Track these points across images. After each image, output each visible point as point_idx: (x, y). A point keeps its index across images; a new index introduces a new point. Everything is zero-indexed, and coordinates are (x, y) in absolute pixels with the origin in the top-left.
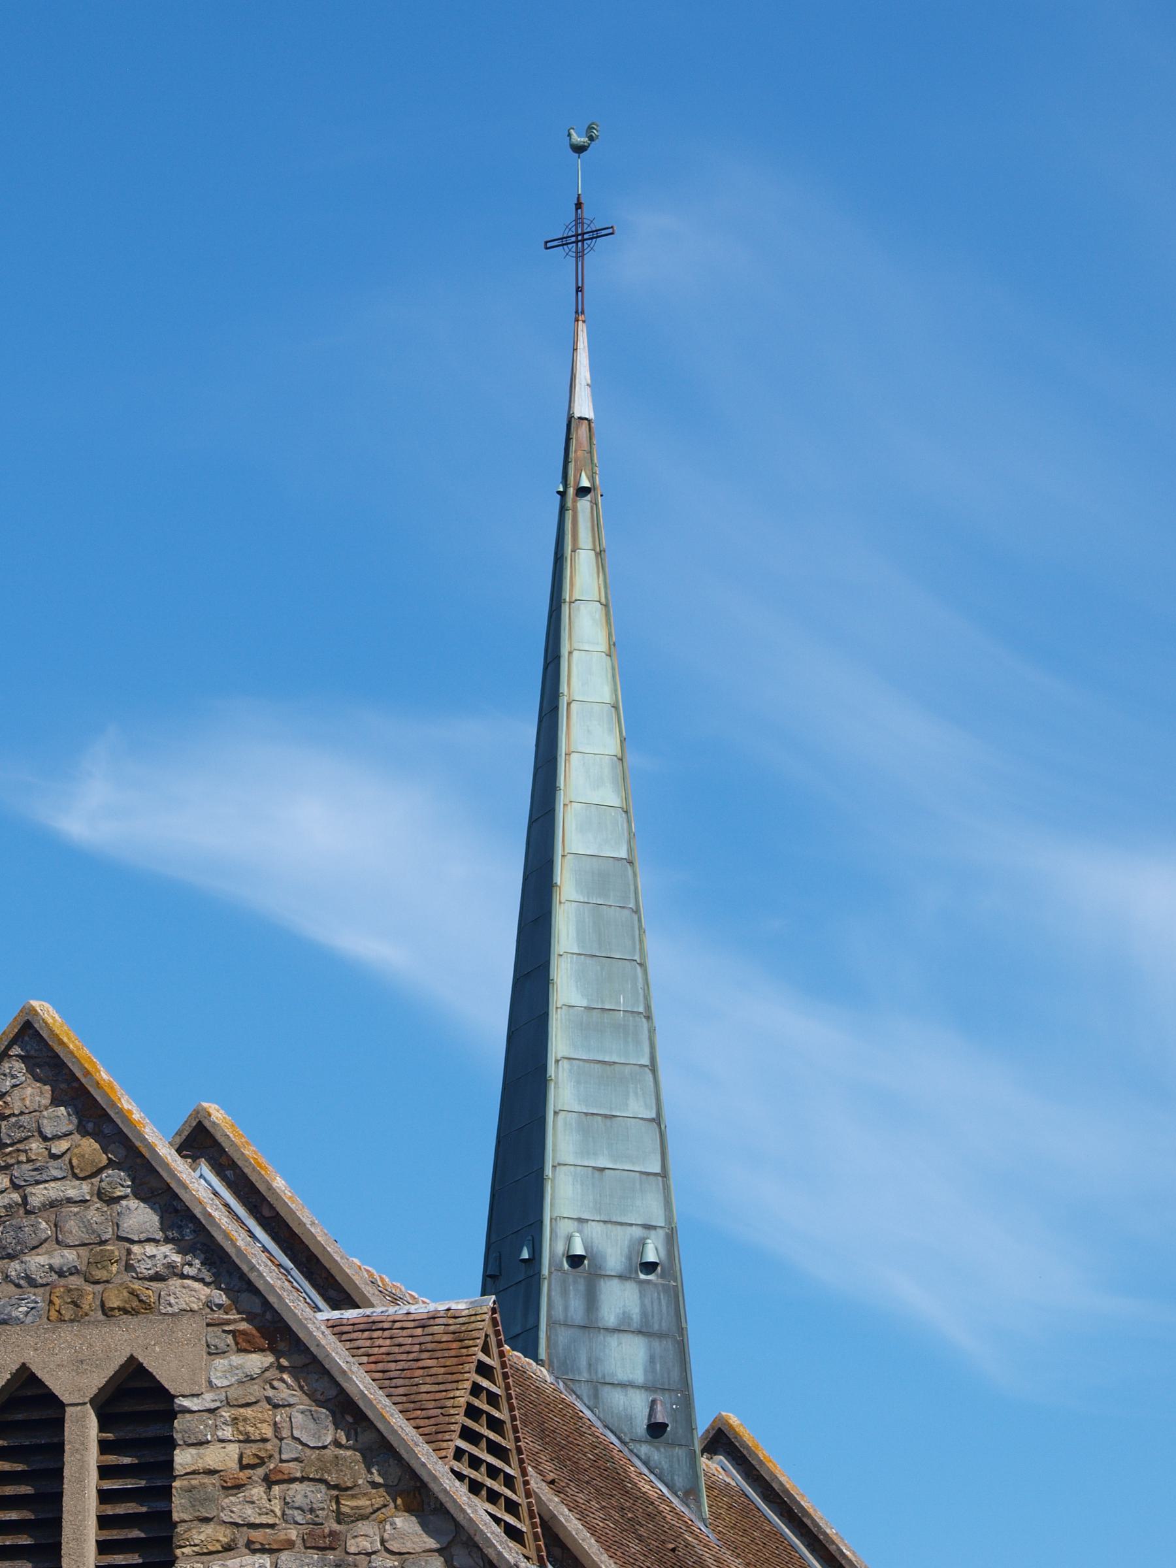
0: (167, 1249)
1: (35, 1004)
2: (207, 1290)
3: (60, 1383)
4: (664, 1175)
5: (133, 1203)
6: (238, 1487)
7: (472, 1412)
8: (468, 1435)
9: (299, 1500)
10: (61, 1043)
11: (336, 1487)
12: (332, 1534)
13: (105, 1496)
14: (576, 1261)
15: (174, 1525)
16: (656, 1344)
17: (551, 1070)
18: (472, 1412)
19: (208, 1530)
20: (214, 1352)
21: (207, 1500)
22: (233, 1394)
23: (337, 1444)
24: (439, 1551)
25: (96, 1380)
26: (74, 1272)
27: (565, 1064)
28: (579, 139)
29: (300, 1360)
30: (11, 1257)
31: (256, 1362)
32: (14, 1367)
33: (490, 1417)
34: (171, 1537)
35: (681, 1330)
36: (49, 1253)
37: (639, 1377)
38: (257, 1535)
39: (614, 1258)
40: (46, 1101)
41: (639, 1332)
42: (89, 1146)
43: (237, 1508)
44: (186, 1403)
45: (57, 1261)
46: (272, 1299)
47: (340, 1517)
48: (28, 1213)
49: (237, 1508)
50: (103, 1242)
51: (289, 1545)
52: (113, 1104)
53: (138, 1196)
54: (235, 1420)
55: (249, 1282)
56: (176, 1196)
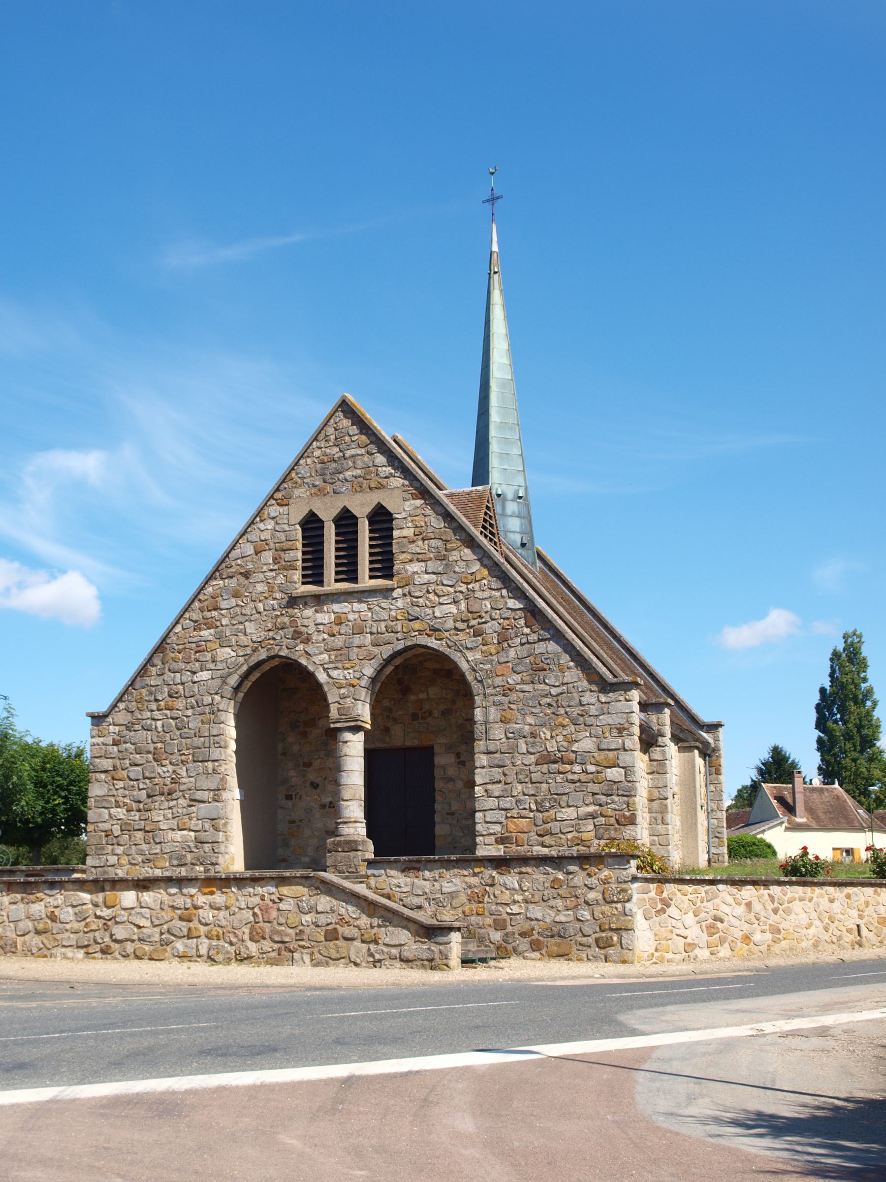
0: (389, 468)
1: (346, 394)
2: (403, 481)
3: (356, 511)
4: (524, 471)
5: (378, 455)
6: (414, 542)
7: (485, 520)
8: (483, 527)
9: (433, 545)
10: (354, 406)
11: (445, 541)
12: (444, 555)
13: (371, 546)
14: (499, 495)
15: (394, 554)
16: (523, 520)
17: (490, 440)
18: (485, 520)
19: (404, 555)
20: (405, 500)
21: (404, 546)
22: (411, 513)
23: (445, 527)
24: (478, 560)
25: (368, 510)
26: (360, 476)
27: (494, 438)
28: (491, 170)
29: (432, 501)
30: (340, 473)
31: (419, 502)
32: (342, 507)
33: (490, 523)
34: (392, 559)
35: (530, 516)
36: (352, 471)
37: (518, 530)
38: (420, 556)
39: (510, 495)
40: (350, 424)
41: (518, 517)
42: (364, 438)
43: (413, 548)
44: (396, 516)
45: (354, 474)
46: (423, 482)
47: (446, 550)
48: (345, 459)
49: (413, 548)
50: (369, 467)
51: (430, 559)
52: (371, 424)
53: (379, 452)
54: (412, 521)
55: (416, 477)
56: (392, 452)
